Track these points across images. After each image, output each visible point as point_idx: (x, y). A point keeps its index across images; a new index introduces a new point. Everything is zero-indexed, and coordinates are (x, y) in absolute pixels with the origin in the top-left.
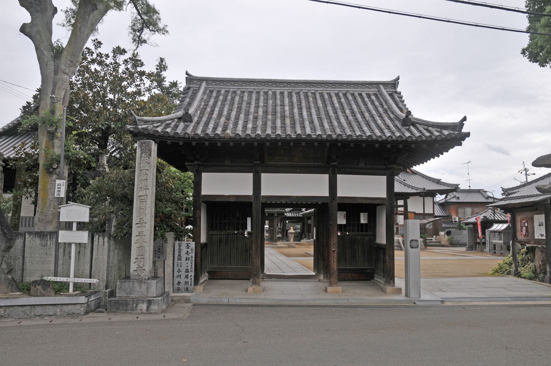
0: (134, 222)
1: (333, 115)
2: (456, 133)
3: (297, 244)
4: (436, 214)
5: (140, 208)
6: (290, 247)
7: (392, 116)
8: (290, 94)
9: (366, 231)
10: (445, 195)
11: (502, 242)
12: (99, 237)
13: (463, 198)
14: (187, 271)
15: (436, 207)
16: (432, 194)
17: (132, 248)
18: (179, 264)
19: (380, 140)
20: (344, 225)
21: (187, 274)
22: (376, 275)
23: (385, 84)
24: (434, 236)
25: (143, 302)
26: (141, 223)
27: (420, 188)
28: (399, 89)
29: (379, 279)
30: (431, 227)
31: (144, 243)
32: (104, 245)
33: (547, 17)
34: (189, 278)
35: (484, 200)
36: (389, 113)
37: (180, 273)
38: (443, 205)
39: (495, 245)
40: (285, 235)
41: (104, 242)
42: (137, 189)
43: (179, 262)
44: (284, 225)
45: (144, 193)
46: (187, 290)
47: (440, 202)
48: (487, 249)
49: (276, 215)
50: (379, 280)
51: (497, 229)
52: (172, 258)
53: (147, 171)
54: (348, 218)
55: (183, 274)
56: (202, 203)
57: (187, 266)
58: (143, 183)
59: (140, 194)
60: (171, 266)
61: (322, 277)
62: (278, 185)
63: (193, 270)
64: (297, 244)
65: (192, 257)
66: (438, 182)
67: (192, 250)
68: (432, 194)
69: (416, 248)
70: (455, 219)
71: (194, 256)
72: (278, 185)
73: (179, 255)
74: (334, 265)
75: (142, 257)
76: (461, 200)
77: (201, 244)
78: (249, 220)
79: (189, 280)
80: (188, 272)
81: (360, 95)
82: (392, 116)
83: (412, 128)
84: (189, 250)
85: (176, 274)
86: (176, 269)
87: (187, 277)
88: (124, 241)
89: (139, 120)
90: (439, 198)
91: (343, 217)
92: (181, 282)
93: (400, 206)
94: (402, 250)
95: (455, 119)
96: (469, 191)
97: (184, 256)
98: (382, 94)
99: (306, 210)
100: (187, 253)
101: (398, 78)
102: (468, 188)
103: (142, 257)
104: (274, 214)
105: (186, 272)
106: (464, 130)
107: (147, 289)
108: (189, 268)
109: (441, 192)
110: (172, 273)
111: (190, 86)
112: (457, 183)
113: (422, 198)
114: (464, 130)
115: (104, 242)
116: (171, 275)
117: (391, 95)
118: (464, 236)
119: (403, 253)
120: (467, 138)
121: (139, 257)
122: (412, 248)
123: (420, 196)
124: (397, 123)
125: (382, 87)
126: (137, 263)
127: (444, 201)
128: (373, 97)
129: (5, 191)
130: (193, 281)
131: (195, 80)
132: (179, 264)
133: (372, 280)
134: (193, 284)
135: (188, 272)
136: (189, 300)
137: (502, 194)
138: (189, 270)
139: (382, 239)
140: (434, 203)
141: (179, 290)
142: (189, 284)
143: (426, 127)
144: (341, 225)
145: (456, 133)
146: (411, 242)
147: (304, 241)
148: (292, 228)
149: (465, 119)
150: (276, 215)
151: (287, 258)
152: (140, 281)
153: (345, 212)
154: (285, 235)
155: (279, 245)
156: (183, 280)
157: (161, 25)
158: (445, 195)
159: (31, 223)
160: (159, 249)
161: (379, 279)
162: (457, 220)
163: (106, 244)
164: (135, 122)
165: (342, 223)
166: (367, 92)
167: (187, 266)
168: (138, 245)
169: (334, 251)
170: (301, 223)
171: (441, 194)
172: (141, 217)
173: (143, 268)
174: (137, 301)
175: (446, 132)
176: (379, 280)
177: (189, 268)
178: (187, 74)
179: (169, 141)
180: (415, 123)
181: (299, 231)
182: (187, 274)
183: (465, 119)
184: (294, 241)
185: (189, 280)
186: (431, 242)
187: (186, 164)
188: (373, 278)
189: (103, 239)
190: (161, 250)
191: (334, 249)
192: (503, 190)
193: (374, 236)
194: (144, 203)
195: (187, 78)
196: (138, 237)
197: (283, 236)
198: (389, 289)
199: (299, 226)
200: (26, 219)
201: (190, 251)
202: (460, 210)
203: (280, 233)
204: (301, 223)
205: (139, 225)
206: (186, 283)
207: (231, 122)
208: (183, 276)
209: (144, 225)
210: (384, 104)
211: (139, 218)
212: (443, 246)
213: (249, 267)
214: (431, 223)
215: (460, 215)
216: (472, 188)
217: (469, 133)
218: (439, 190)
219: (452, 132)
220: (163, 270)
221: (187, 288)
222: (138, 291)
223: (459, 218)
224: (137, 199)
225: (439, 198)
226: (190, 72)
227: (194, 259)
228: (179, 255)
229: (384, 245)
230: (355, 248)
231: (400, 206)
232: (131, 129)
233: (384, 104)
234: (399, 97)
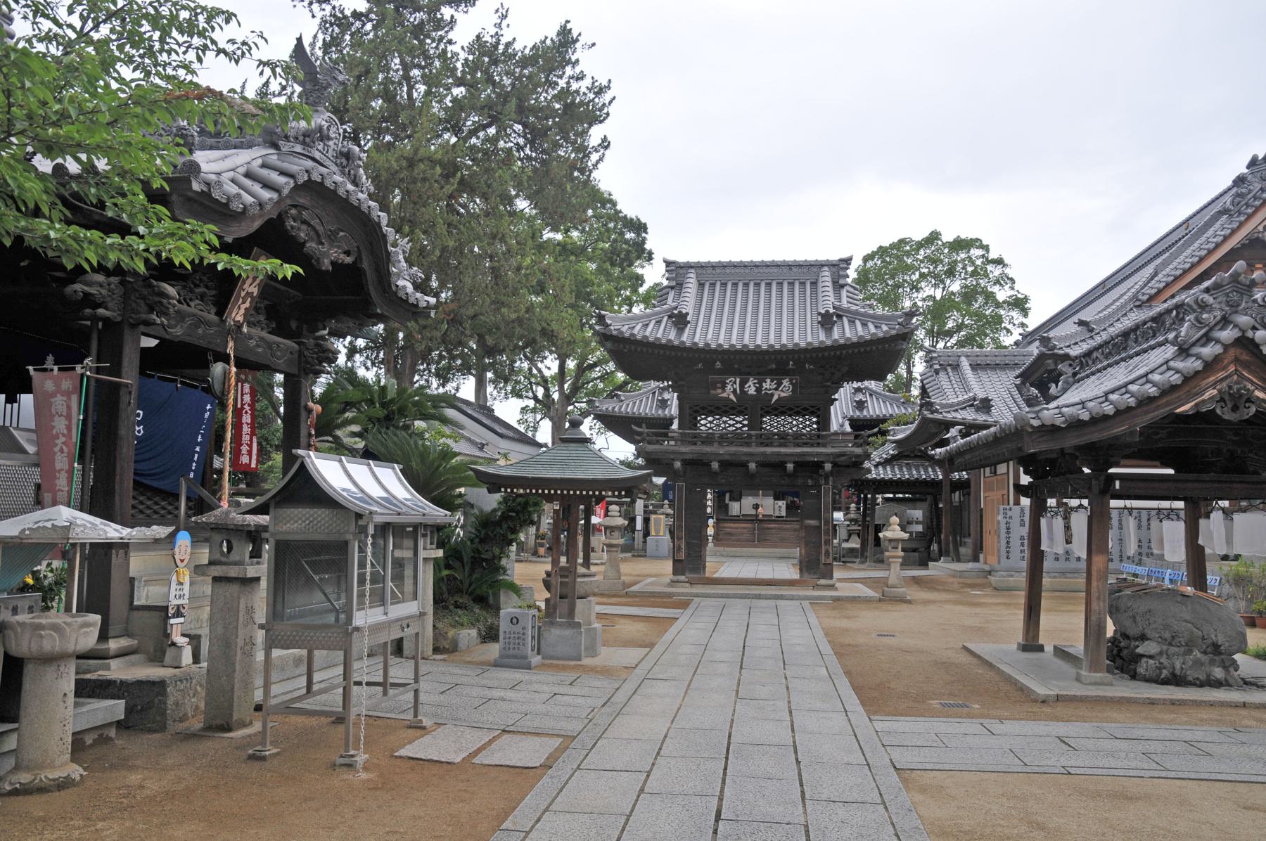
3: (916, 581)
6: (888, 598)
33: (490, 389)
40: (870, 543)
44: (869, 508)
49: (828, 467)
64: (916, 581)
78: (1171, 471)
99: (221, 455)
104: (819, 465)
129: (1055, 647)
147: (940, 568)
148: (895, 519)
150: (828, 467)
154: (870, 543)
155: (845, 590)
157: (605, 83)
170: (926, 505)
181: (920, 528)
184: (905, 564)
197: (864, 544)
199: (917, 514)
203: (855, 537)
204: (926, 505)
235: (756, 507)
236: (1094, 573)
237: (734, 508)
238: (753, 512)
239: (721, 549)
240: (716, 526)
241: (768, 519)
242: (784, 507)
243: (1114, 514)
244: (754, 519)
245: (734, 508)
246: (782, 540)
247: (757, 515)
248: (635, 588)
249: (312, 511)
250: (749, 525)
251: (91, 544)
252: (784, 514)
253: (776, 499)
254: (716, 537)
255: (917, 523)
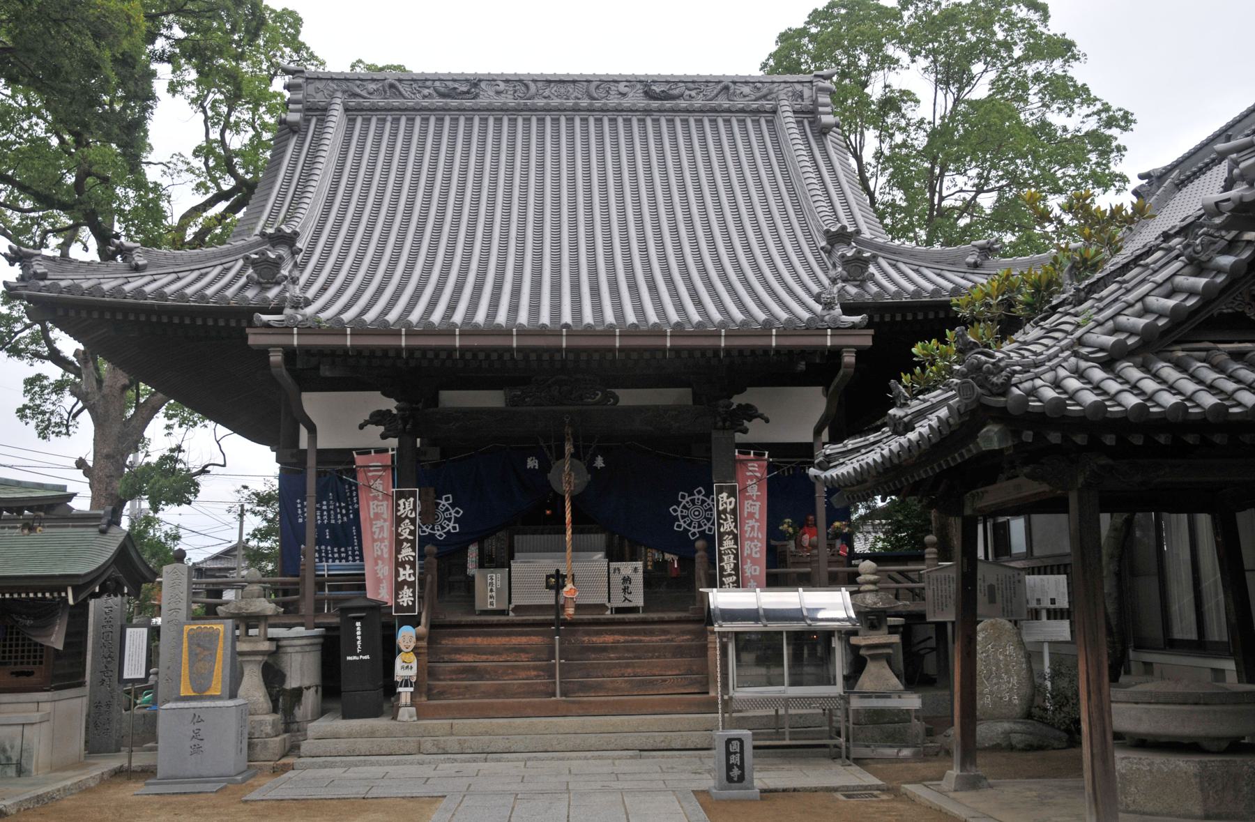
235: (556, 581)
236: (1153, 529)
237: (490, 588)
238: (548, 598)
239: (438, 724)
240: (428, 650)
241: (593, 619)
242: (638, 579)
243: (821, 492)
244: (551, 621)
245: (490, 588)
246: (644, 685)
247: (558, 608)
248: (1113, 622)
249: (953, 597)
250: (536, 640)
251: (338, 637)
252: (638, 600)
253: (614, 555)
254: (423, 687)
255: (1055, 614)
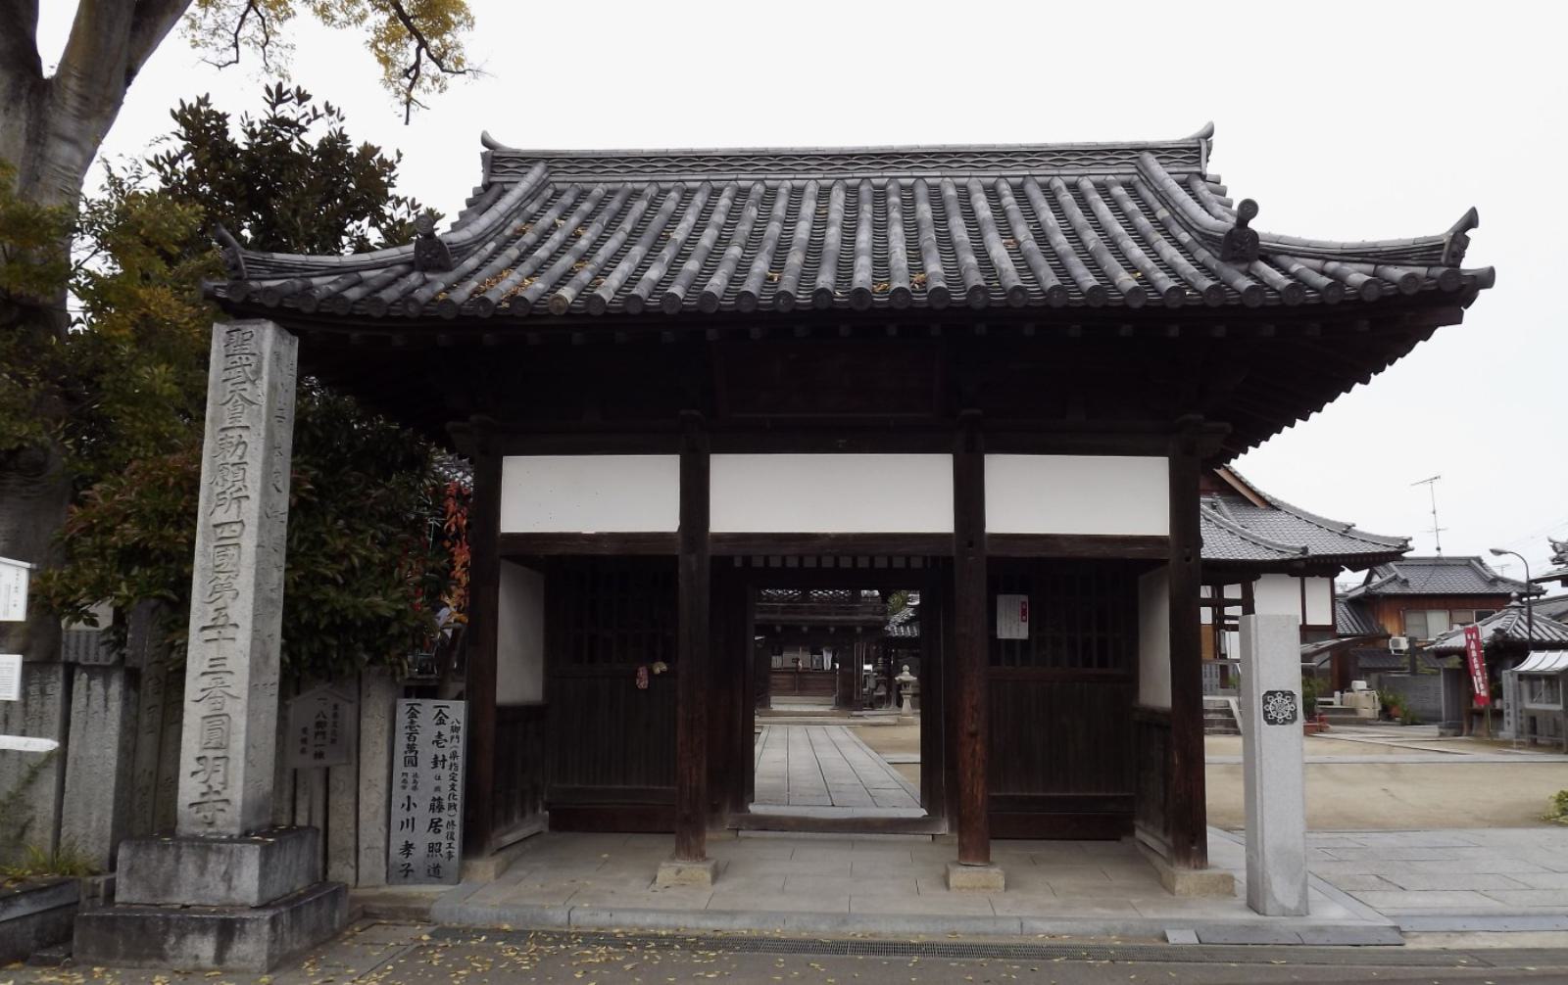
0: (195, 623)
1: (966, 237)
2: (1439, 271)
4: (1340, 631)
5: (217, 569)
7: (1185, 237)
8: (824, 194)
9: (1103, 664)
10: (1364, 573)
11: (1559, 707)
12: (90, 679)
13: (1419, 584)
14: (437, 805)
15: (1341, 608)
16: (1326, 567)
17: (186, 721)
18: (410, 779)
19: (1137, 304)
20: (1022, 641)
21: (437, 815)
22: (1139, 823)
23: (1165, 152)
24: (1337, 694)
25: (203, 928)
26: (220, 624)
27: (1293, 548)
28: (1211, 169)
29: (1148, 837)
30: (1327, 665)
31: (228, 701)
32: (106, 708)
34: (444, 831)
35: (1480, 588)
36: (1176, 229)
37: (414, 811)
38: (1363, 604)
39: (1533, 719)
41: (106, 700)
42: (209, 501)
43: (410, 770)
45: (232, 516)
46: (435, 873)
47: (1352, 595)
48: (1508, 732)
50: (1150, 841)
51: (1541, 667)
52: (383, 759)
53: (245, 433)
54: (1036, 617)
55: (423, 814)
56: (503, 561)
57: (437, 789)
58: (230, 478)
59: (220, 516)
60: (383, 785)
61: (944, 828)
62: (771, 496)
63: (459, 803)
65: (454, 755)
66: (1347, 531)
67: (455, 729)
68: (1326, 567)
69: (1285, 721)
70: (1396, 643)
71: (460, 752)
72: (771, 496)
73: (411, 748)
74: (977, 789)
75: (220, 753)
76: (1415, 588)
77: (503, 710)
79: (442, 838)
80: (441, 808)
81: (1073, 187)
82: (1185, 237)
83: (1263, 267)
84: (446, 730)
85: (399, 814)
86: (399, 798)
87: (435, 826)
88: (156, 688)
89: (248, 261)
90: (1350, 580)
91: (1017, 616)
92: (416, 844)
93: (1233, 603)
94: (1237, 733)
95: (1437, 226)
96: (1439, 564)
97: (426, 751)
98: (1148, 180)
100: (438, 740)
101: (1209, 134)
102: (1434, 554)
103: (220, 753)
105: (432, 808)
106: (1471, 262)
107: (227, 878)
108: (444, 794)
109: (1355, 562)
110: (382, 811)
111: (494, 179)
112: (1406, 536)
113: (1298, 579)
114: (1471, 262)
115: (106, 700)
116: (381, 819)
117: (1185, 185)
118: (1437, 693)
119: (1236, 742)
120: (1482, 293)
121: (210, 754)
122: (1272, 722)
123: (1292, 575)
124: (1203, 254)
125: (1150, 160)
126: (201, 777)
127: (1362, 591)
128: (1118, 191)
130: (456, 844)
131: (511, 159)
132: (410, 779)
133: (1125, 839)
134: (456, 852)
135: (441, 808)
136: (425, 912)
137: (1553, 560)
138: (445, 803)
139: (1158, 690)
140: (1334, 597)
141: (407, 872)
142: (444, 851)
143: (1318, 263)
144: (1010, 642)
145: (1439, 271)
146: (1266, 702)
148: (906, 667)
149: (1471, 220)
150: (859, 630)
151: (829, 753)
152: (204, 846)
153: (1024, 598)
156: (422, 838)
158: (1364, 573)
159: (219, 662)
160: (319, 724)
161: (1148, 837)
162: (1404, 645)
163: (115, 706)
164: (236, 267)
165: (1015, 636)
166: (1100, 179)
167: (437, 789)
168: (204, 709)
169: (973, 735)
171: (1355, 568)
172: (220, 604)
173: (225, 795)
174: (189, 921)
175: (1397, 273)
176: (1150, 841)
177: (444, 794)
178: (485, 142)
179: (355, 335)
180: (1272, 254)
182: (437, 815)
183: (1471, 220)
185: (442, 838)
186: (1327, 711)
187: (449, 425)
188: (1130, 831)
189: (106, 686)
190: (328, 729)
191: (973, 728)
192: (1555, 548)
193: (1130, 680)
194: (232, 551)
195: (484, 156)
196: (207, 678)
198: (1186, 878)
200: (78, 637)
201: (447, 734)
202: (1413, 619)
205: (212, 634)
206: (433, 848)
207: (590, 266)
208: (422, 825)
209: (229, 632)
210: (1157, 205)
211: (211, 608)
212: (1364, 722)
213: (699, 792)
214: (1327, 655)
215: (1413, 632)
216: (1445, 553)
217: (1492, 271)
218: (1350, 556)
219: (1422, 271)
220: (352, 800)
221: (437, 868)
222: (196, 884)
223: (1411, 641)
224: (206, 539)
225: (1350, 580)
226: (497, 138)
227: (460, 761)
228: (411, 748)
229: (1165, 714)
230: (1072, 718)
231: (1233, 603)
232: (221, 294)
233: (1157, 205)
234: (1213, 191)
